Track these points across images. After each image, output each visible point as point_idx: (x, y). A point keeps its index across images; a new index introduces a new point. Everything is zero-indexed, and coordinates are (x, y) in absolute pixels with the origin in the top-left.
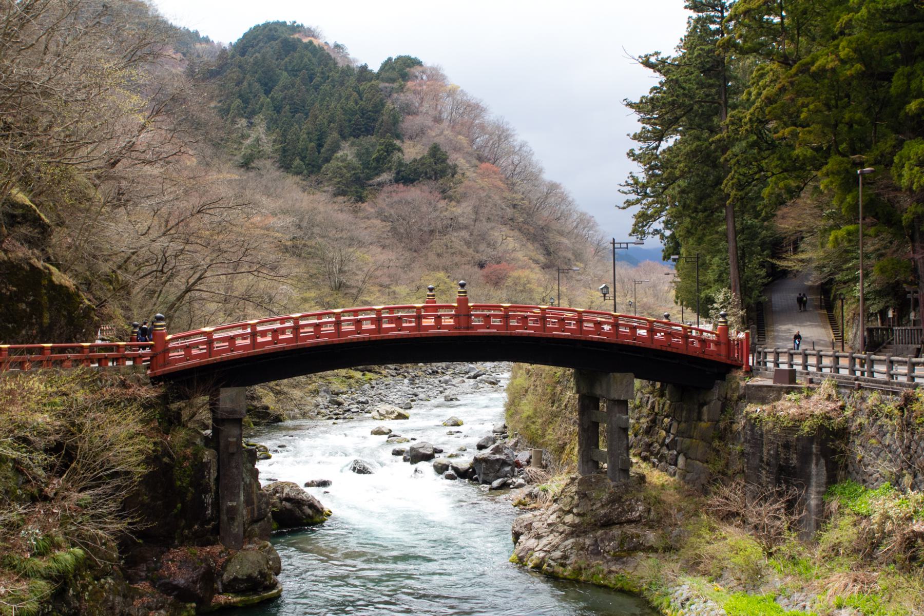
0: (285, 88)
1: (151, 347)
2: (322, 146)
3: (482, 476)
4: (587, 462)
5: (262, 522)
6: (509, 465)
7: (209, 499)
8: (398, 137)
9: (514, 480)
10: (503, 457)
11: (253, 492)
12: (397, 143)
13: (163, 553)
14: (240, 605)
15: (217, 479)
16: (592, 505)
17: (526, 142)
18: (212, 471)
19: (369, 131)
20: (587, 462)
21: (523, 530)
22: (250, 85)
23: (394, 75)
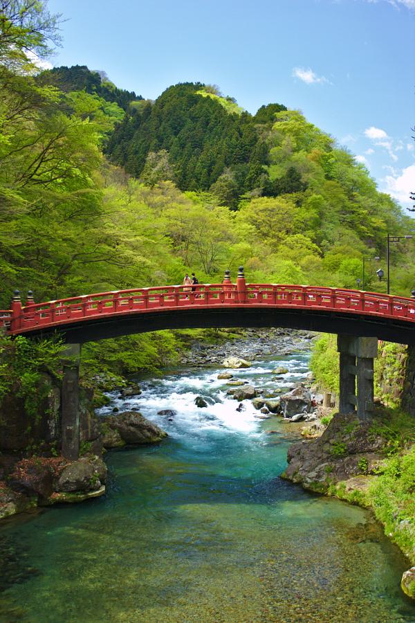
0: (189, 130)
1: (11, 313)
2: (212, 171)
3: (286, 411)
4: (346, 404)
5: (95, 441)
6: (306, 404)
7: (52, 424)
8: (267, 163)
9: (309, 415)
10: (301, 398)
11: (87, 420)
12: (265, 167)
13: (16, 461)
14: (70, 501)
15: (60, 409)
16: (343, 438)
17: (364, 165)
18: (55, 404)
19: (245, 159)
20: (346, 404)
21: (295, 454)
22: (164, 128)
23: (266, 118)
